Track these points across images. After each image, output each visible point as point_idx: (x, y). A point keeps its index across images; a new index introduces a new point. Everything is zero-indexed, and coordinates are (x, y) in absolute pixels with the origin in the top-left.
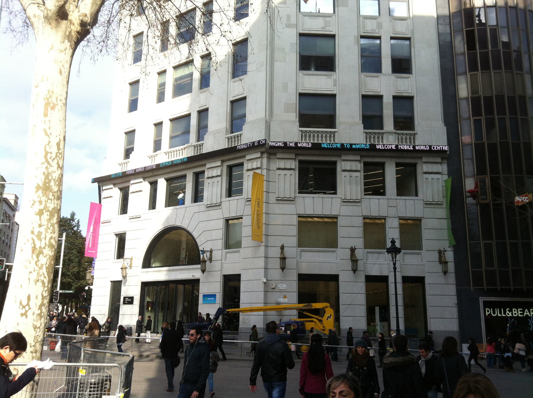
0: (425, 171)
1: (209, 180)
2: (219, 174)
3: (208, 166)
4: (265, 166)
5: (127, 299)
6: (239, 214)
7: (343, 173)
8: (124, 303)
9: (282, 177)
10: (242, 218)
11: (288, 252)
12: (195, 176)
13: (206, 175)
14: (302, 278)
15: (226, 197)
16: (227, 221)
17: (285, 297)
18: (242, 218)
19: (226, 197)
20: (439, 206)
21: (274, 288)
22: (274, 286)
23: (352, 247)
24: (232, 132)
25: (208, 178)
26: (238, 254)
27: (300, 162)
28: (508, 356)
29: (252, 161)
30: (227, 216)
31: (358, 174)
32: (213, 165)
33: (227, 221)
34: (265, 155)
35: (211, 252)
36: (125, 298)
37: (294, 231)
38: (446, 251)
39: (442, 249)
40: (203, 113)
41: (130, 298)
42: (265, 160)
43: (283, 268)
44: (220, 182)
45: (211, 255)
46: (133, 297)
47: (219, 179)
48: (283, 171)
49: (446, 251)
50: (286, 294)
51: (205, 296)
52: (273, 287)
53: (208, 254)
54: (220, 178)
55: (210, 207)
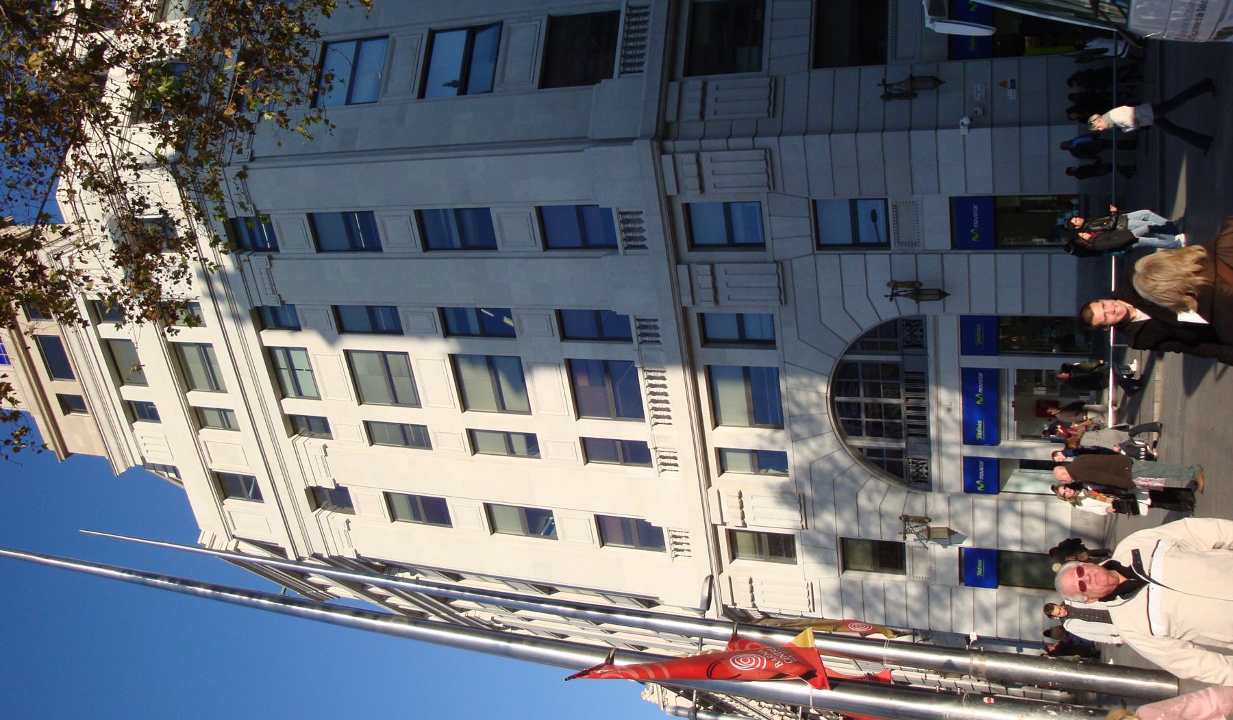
0: (697, 117)
1: (722, 298)
4: (694, 144)
7: (707, 117)
10: (814, 202)
16: (820, 246)
20: (781, 85)
21: (984, 110)
22: (977, 109)
23: (883, 97)
24: (616, 247)
27: (688, 73)
29: (680, 176)
30: (807, 245)
31: (711, 86)
33: (820, 246)
34: (669, 144)
37: (847, 75)
38: (884, 81)
39: (881, 90)
40: (568, 325)
42: (680, 145)
47: (719, 269)
48: (704, 166)
49: (884, 81)
52: (980, 112)
54: (717, 266)
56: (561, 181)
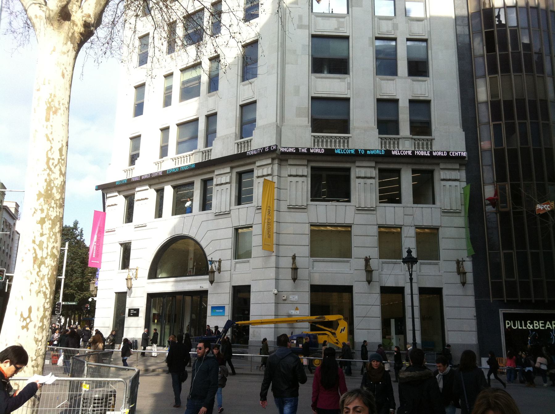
0: (442, 178)
1: (218, 187)
2: (228, 181)
3: (217, 172)
4: (276, 173)
5: (132, 311)
6: (249, 223)
7: (357, 180)
8: (129, 315)
9: (294, 184)
10: (252, 227)
11: (300, 262)
12: (203, 183)
13: (215, 182)
14: (314, 289)
15: (235, 205)
16: (236, 229)
17: (297, 309)
18: (252, 227)
19: (235, 205)
20: (457, 215)
21: (285, 300)
22: (285, 297)
23: (366, 257)
25: (217, 185)
26: (248, 264)
27: (313, 168)
28: (529, 371)
29: (263, 167)
30: (236, 224)
31: (372, 181)
32: (222, 171)
33: (236, 229)
34: (276, 161)
35: (220, 262)
36: (130, 310)
37: (306, 240)
38: (464, 261)
39: (460, 259)
41: (135, 310)
42: (276, 167)
43: (294, 279)
44: (229, 189)
45: (220, 266)
46: (139, 309)
47: (228, 186)
48: (295, 178)
49: (464, 261)
50: (298, 306)
51: (213, 308)
52: (284, 298)
53: (217, 264)
54: (229, 185)
55: (218, 215)
56: (265, 116)
